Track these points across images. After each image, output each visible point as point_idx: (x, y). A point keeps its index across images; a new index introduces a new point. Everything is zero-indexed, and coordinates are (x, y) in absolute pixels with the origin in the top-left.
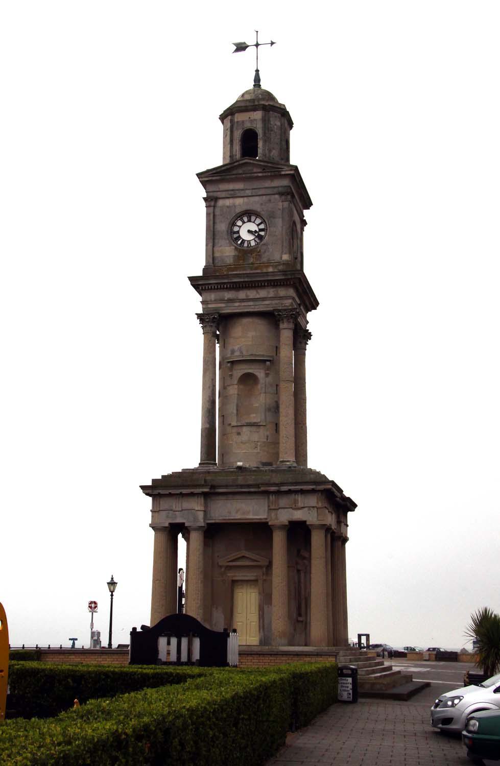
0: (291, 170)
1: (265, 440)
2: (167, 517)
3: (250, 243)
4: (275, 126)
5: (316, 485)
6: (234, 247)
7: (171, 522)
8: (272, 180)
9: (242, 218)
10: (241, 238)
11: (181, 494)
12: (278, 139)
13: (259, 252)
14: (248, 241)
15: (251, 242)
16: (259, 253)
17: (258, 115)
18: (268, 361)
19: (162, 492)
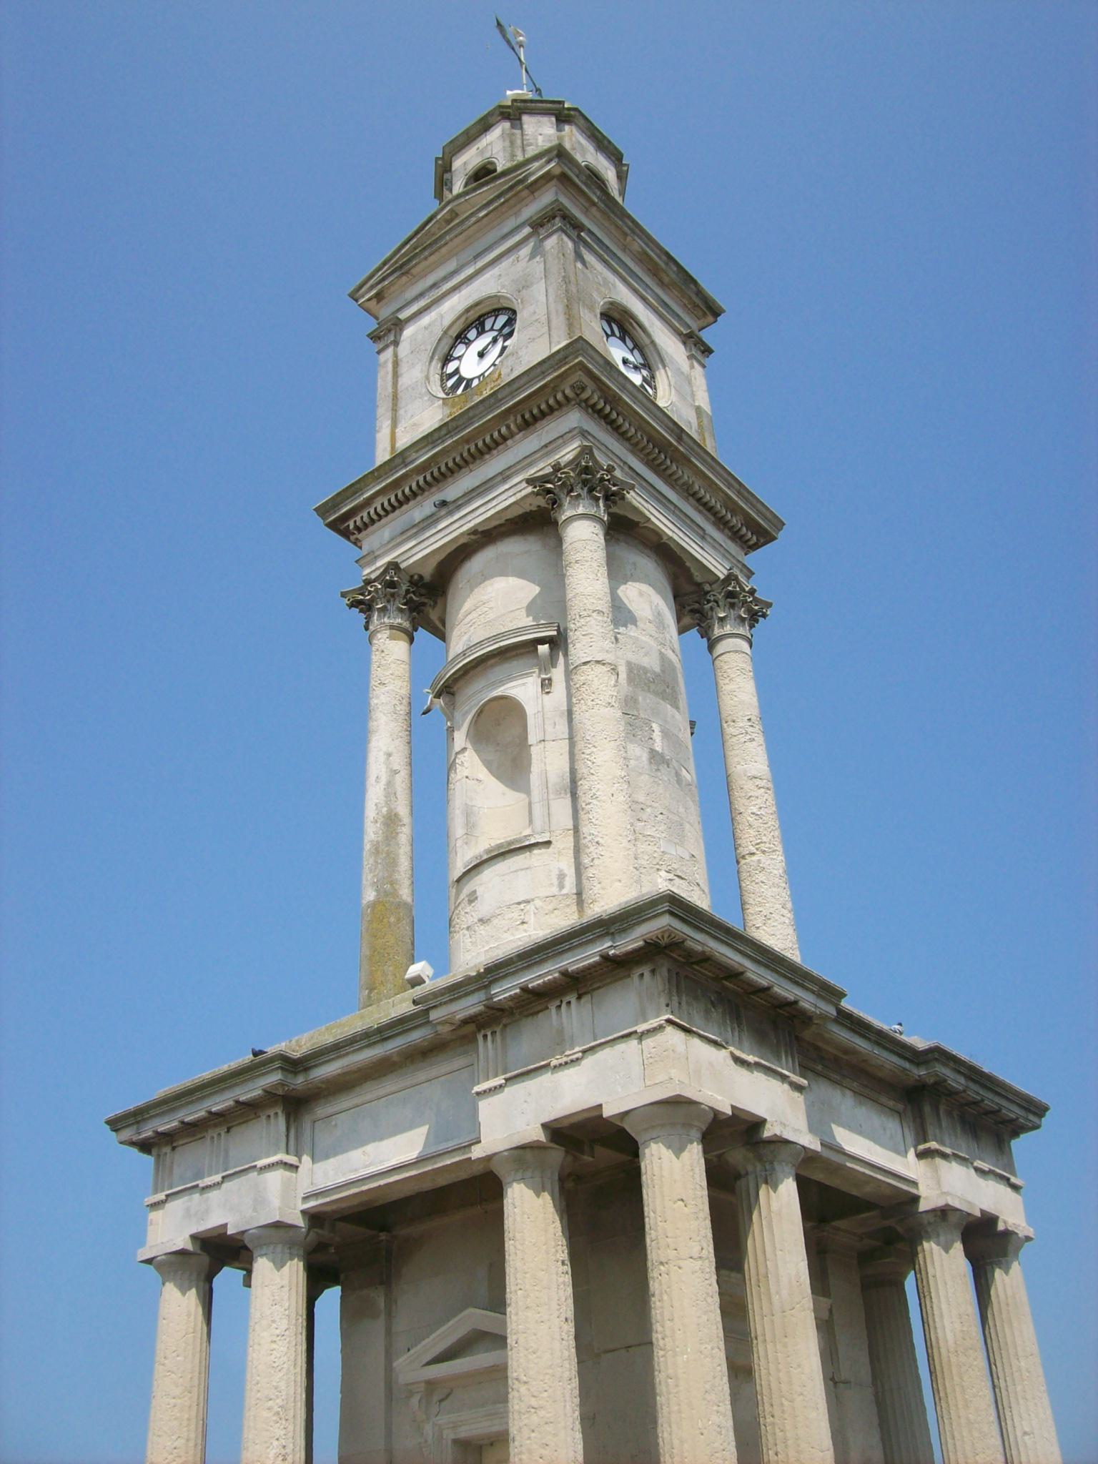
1: (555, 890)
5: (612, 935)
18: (542, 641)
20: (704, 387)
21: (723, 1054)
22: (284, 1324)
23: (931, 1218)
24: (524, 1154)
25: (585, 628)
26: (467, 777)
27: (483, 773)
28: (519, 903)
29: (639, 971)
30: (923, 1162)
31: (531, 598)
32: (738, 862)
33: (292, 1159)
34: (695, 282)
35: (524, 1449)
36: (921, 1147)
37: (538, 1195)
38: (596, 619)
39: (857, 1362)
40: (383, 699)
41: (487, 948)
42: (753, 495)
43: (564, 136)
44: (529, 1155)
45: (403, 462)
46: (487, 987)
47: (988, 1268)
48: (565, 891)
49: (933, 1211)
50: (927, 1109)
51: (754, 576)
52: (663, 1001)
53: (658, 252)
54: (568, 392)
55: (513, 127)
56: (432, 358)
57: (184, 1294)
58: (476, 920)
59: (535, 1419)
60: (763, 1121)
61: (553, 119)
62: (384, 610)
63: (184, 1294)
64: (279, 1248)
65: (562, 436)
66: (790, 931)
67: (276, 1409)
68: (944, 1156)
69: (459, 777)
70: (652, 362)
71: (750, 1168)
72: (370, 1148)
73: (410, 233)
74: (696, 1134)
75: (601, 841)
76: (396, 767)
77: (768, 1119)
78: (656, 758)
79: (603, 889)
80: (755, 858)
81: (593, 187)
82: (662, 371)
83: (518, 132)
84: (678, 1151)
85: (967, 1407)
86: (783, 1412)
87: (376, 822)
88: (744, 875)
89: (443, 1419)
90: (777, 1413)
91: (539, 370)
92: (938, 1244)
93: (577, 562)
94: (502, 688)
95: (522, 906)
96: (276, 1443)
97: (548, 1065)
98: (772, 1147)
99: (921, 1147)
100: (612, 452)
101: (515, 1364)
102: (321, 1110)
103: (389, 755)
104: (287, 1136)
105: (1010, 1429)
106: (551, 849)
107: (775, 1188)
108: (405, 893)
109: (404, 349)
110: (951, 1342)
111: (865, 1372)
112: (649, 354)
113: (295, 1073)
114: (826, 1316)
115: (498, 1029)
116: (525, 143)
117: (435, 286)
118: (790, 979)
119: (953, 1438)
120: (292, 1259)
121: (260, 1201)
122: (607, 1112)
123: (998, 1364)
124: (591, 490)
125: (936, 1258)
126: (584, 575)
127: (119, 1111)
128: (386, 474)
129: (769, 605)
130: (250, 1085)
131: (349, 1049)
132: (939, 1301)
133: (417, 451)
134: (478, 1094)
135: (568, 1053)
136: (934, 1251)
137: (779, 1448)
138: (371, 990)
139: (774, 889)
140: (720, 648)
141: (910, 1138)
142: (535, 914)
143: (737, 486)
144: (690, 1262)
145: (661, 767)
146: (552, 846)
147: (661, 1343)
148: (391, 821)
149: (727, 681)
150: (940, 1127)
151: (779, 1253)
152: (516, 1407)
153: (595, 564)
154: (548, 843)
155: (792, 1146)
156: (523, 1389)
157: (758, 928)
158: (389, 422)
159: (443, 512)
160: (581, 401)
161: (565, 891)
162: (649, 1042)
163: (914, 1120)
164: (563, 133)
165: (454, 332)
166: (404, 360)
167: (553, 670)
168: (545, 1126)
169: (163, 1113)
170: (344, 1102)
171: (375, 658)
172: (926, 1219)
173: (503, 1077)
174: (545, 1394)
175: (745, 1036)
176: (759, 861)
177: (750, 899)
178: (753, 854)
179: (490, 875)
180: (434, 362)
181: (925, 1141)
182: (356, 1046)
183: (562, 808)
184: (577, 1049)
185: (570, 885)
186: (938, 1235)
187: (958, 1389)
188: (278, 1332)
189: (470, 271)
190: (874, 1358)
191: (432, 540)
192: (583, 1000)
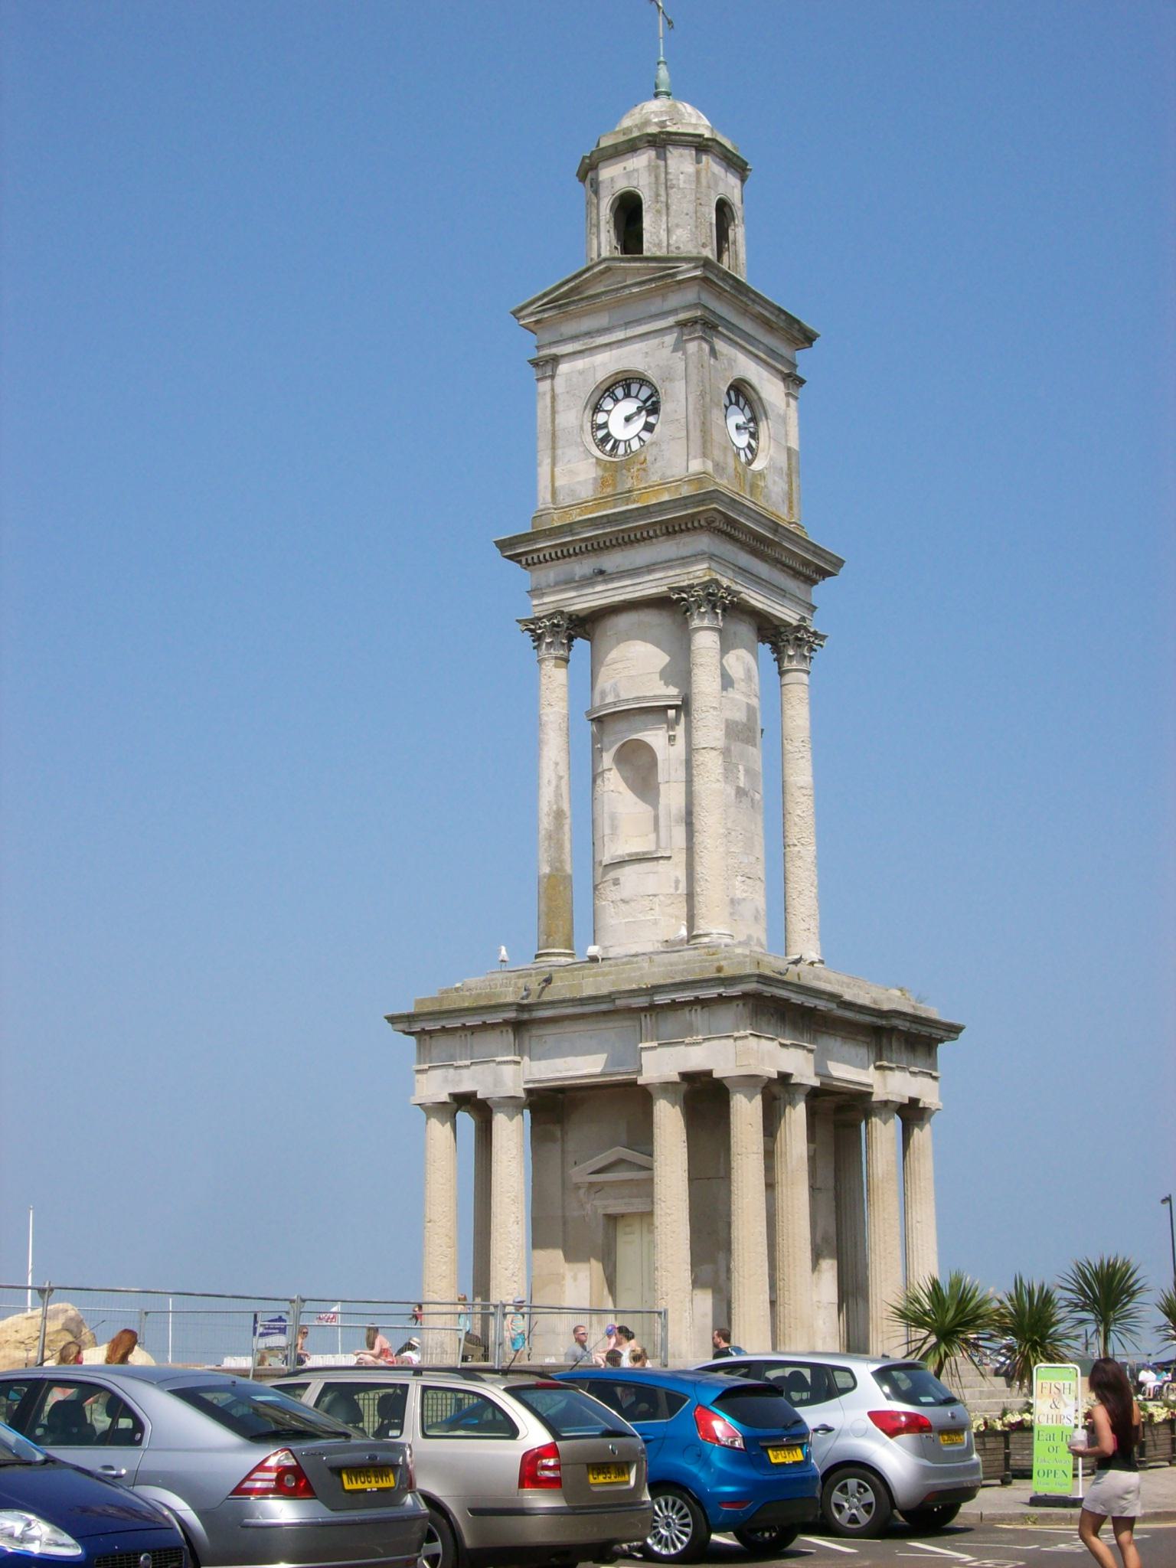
0: (695, 268)
1: (672, 890)
2: (446, 1080)
3: (629, 445)
4: (681, 177)
5: (725, 986)
6: (594, 460)
7: (451, 1091)
8: (664, 297)
9: (613, 393)
10: (613, 437)
11: (464, 1027)
12: (689, 201)
13: (642, 463)
14: (625, 441)
15: (632, 442)
16: (644, 466)
17: (642, 160)
18: (671, 707)
19: (430, 1026)
20: (796, 423)
21: (776, 1043)
22: (515, 1152)
23: (878, 1105)
24: (667, 1087)
25: (704, 721)
26: (612, 791)
27: (623, 787)
28: (649, 896)
29: (738, 1003)
30: (878, 1072)
31: (662, 666)
32: (785, 848)
33: (517, 1058)
34: (798, 322)
35: (663, 1233)
36: (878, 1063)
37: (673, 1107)
38: (713, 715)
39: (827, 1199)
40: (552, 718)
41: (627, 920)
42: (824, 550)
43: (701, 169)
44: (670, 1087)
45: (571, 531)
46: (652, 995)
47: (911, 1127)
48: (678, 892)
49: (881, 1102)
50: (885, 1041)
51: (817, 610)
52: (749, 1022)
53: (772, 309)
54: (703, 523)
55: (658, 157)
56: (585, 407)
57: (443, 1126)
58: (619, 899)
59: (669, 1219)
60: (792, 1075)
61: (694, 152)
62: (550, 644)
63: (443, 1126)
64: (511, 1109)
65: (695, 556)
66: (815, 902)
67: (513, 1197)
68: (891, 1069)
69: (606, 789)
70: (758, 415)
71: (782, 1096)
72: (570, 1059)
73: (568, 277)
74: (759, 1090)
75: (709, 879)
76: (562, 774)
77: (795, 1073)
78: (740, 792)
79: (708, 910)
80: (796, 849)
81: (728, 279)
82: (765, 423)
83: (662, 163)
84: (750, 1099)
85: (884, 1210)
86: (788, 1220)
87: (549, 815)
88: (788, 859)
89: (597, 1203)
90: (785, 1221)
91: (682, 502)
92: (880, 1119)
93: (701, 665)
94: (640, 734)
95: (651, 898)
96: (513, 1215)
97: (683, 1042)
98: (795, 1087)
99: (878, 1063)
100: (725, 560)
101: (659, 1192)
102: (535, 1032)
103: (557, 764)
104: (514, 1045)
105: (910, 1219)
106: (671, 861)
107: (794, 1108)
108: (568, 869)
109: (559, 381)
110: (880, 1176)
111: (831, 1183)
112: (756, 407)
113: (522, 1011)
114: (812, 1154)
115: (654, 1014)
116: (669, 183)
117: (589, 334)
118: (814, 997)
119: (875, 1226)
120: (517, 1115)
121: (498, 1081)
122: (716, 1075)
123: (909, 1182)
124: (714, 607)
125: (878, 1128)
126: (706, 677)
127: (396, 1012)
128: (555, 535)
129: (823, 638)
130: (494, 1016)
131: (560, 1005)
132: (877, 1152)
133: (582, 527)
134: (642, 1048)
135: (695, 1038)
136: (878, 1124)
137: (785, 1238)
138: (549, 936)
139: (807, 873)
140: (788, 678)
141: (872, 1057)
142: (659, 905)
143: (812, 548)
144: (752, 1155)
145: (743, 799)
146: (672, 859)
147: (736, 1192)
148: (559, 815)
149: (789, 706)
150: (892, 1050)
151: (793, 1142)
152: (659, 1212)
153: (713, 668)
154: (669, 858)
155: (804, 1087)
156: (663, 1204)
157: (794, 899)
158: (549, 460)
159: (600, 579)
160: (711, 527)
161: (678, 892)
162: (739, 1042)
163: (876, 1045)
164: (701, 165)
165: (604, 387)
166: (560, 396)
167: (677, 727)
168: (680, 1073)
169: (430, 1020)
170: (550, 1030)
171: (544, 681)
172: (875, 1105)
173: (657, 1042)
174: (674, 1208)
175: (787, 1032)
176: (799, 852)
177: (791, 877)
178: (796, 845)
179: (628, 873)
180: (587, 411)
181: (881, 1060)
182: (565, 1005)
183: (679, 833)
184: (700, 1037)
185: (683, 888)
186: (881, 1115)
187: (880, 1201)
188: (512, 1156)
189: (620, 335)
190: (837, 1179)
191: (590, 597)
192: (704, 1010)
